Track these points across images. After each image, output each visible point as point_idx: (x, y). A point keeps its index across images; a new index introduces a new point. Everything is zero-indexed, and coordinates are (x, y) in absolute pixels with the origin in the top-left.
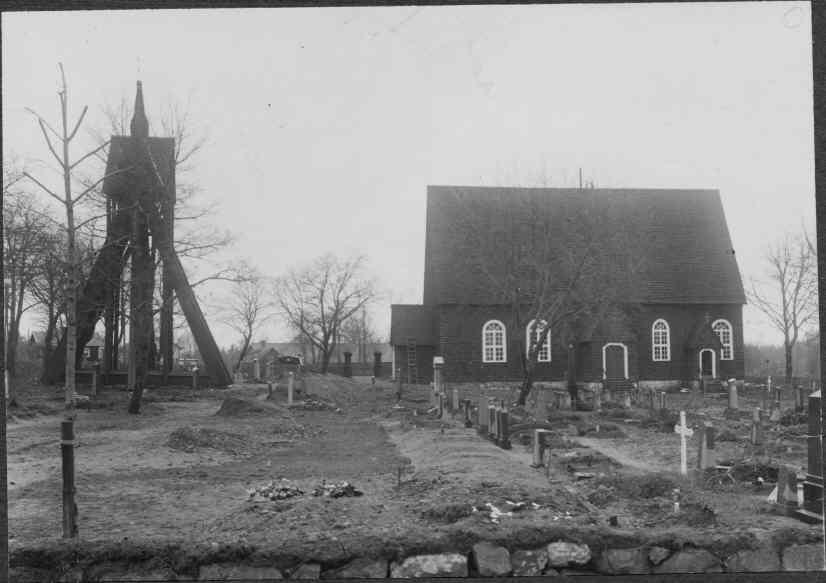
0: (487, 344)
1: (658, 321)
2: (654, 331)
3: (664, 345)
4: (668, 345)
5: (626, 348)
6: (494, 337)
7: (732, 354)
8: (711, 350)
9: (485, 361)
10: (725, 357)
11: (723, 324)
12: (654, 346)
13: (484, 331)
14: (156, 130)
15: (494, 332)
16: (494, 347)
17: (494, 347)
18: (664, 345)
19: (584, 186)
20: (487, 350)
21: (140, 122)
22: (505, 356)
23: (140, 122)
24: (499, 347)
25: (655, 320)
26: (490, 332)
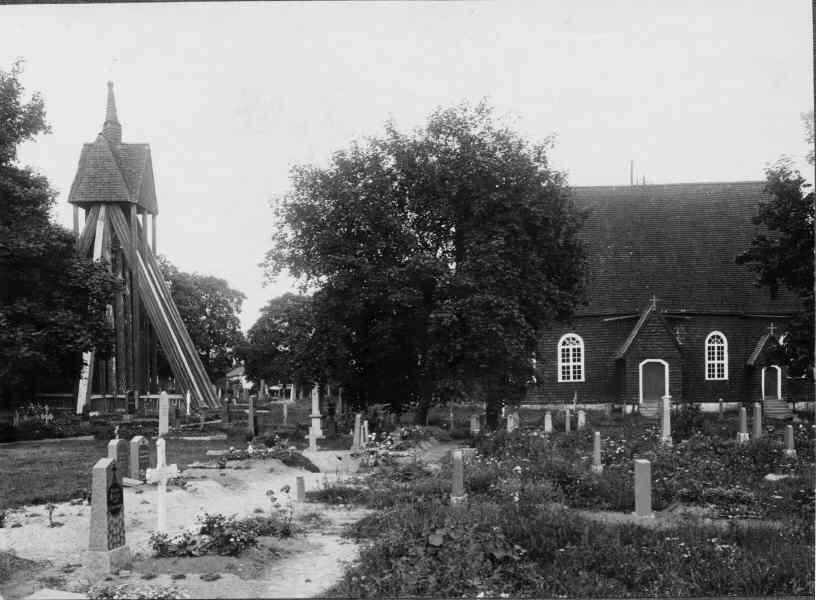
0: (563, 361)
1: (715, 333)
2: (707, 345)
3: (720, 362)
4: (726, 362)
5: (666, 365)
6: (571, 370)
7: (583, 374)
8: (776, 367)
9: (707, 378)
10: (563, 378)
11: (718, 337)
12: (707, 362)
13: (560, 347)
14: (128, 138)
15: (716, 345)
16: (571, 364)
17: (571, 364)
18: (720, 362)
19: (635, 183)
20: (579, 360)
21: (112, 128)
22: (583, 374)
23: (112, 128)
24: (565, 364)
25: (708, 333)
26: (711, 345)
